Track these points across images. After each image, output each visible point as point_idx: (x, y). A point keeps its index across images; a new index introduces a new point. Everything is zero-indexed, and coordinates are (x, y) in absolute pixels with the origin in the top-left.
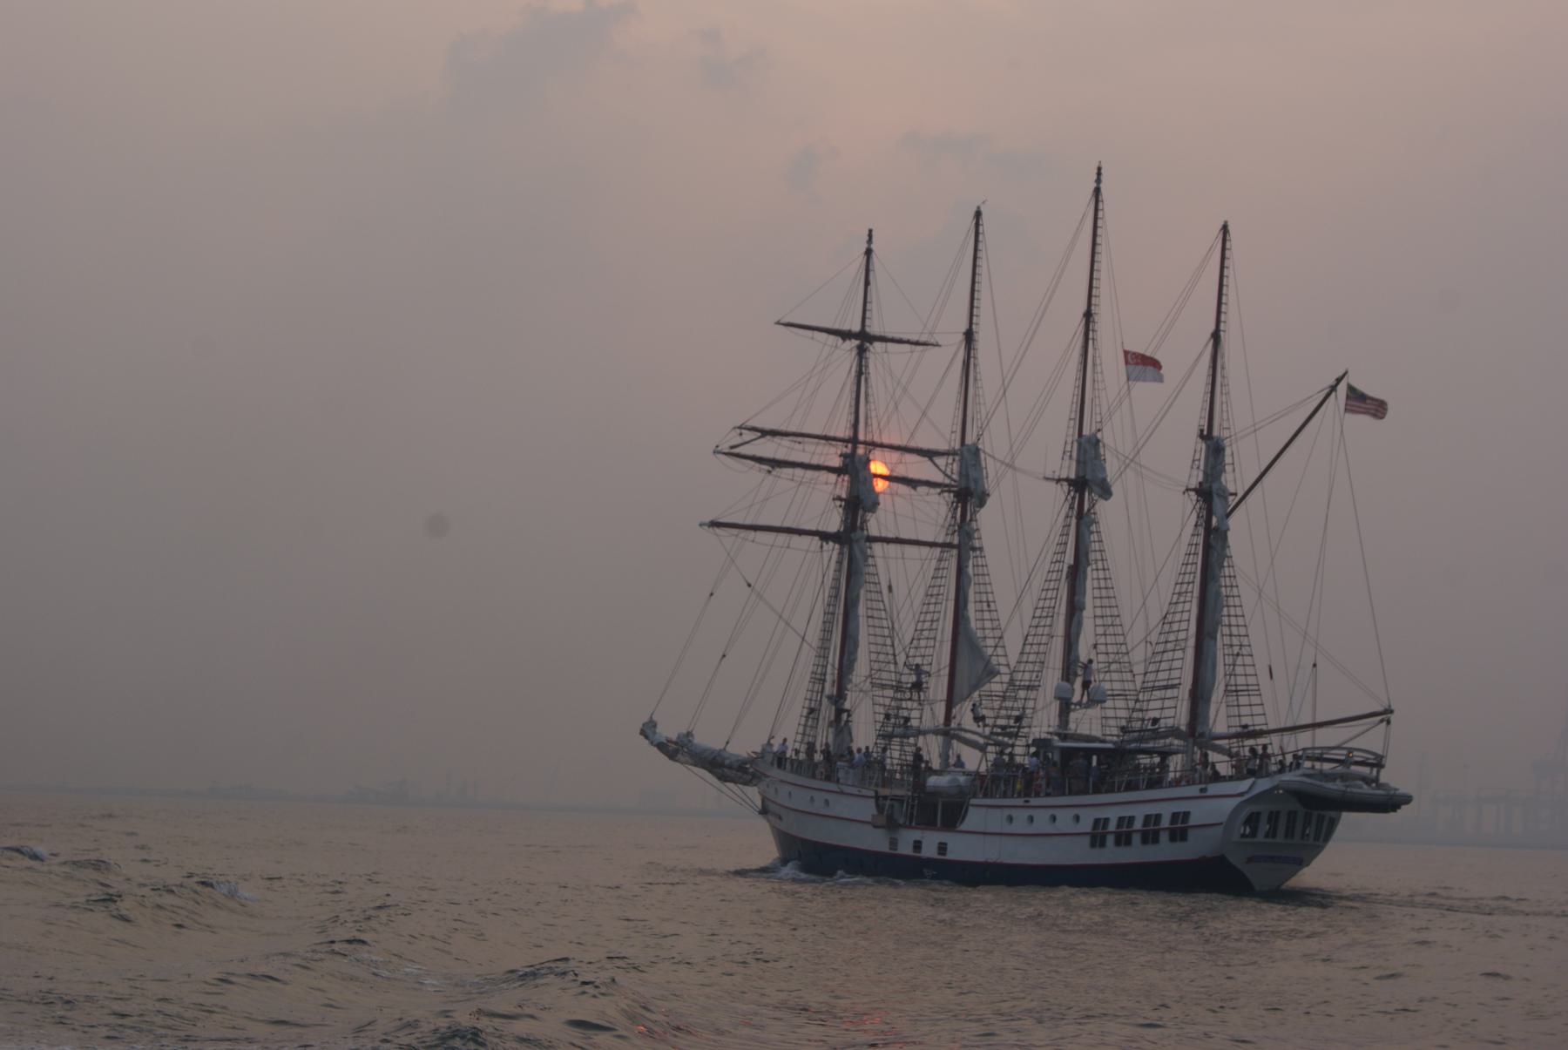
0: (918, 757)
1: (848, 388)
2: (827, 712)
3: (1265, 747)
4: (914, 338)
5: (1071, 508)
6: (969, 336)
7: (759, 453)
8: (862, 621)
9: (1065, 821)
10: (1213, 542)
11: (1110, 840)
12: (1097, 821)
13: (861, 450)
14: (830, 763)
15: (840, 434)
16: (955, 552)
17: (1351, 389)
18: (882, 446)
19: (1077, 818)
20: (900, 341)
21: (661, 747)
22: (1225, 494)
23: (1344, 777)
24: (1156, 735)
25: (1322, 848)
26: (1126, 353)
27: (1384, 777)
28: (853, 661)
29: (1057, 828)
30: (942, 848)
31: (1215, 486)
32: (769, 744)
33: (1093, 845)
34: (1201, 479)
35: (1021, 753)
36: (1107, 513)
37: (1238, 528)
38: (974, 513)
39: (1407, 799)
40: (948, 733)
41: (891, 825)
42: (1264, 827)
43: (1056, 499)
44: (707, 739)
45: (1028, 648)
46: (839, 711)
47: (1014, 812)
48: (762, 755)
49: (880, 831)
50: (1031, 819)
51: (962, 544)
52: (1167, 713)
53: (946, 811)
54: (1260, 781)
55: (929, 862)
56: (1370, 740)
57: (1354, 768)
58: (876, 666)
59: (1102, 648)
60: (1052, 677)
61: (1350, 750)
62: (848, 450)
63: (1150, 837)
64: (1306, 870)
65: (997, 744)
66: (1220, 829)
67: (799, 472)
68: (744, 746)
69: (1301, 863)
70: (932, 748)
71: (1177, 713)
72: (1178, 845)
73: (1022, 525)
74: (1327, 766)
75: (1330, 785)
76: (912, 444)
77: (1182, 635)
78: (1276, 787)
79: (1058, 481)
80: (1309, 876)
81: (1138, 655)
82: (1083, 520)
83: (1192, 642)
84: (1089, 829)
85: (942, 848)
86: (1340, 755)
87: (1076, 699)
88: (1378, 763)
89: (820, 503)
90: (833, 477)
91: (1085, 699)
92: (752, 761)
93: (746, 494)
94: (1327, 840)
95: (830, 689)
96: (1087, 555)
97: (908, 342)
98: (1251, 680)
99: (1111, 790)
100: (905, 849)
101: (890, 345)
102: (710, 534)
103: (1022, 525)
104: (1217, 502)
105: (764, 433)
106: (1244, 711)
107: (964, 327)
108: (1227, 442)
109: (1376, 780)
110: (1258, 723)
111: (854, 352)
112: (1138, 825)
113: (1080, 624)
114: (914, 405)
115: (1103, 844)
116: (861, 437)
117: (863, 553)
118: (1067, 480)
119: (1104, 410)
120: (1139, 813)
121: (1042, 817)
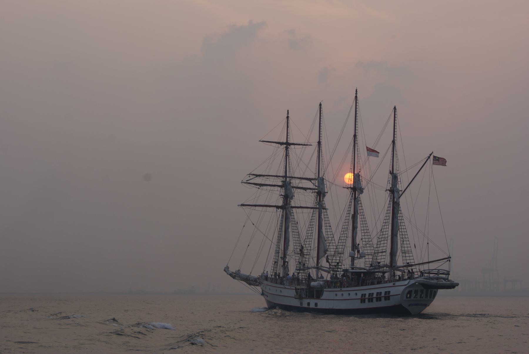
0: (309, 275)
1: (283, 160)
2: (281, 262)
3: (412, 270)
4: (303, 144)
5: (352, 196)
6: (319, 143)
7: (255, 182)
8: (291, 234)
9: (353, 295)
10: (395, 206)
11: (367, 300)
12: (362, 295)
13: (288, 179)
14: (279, 280)
15: (281, 175)
16: (318, 210)
17: (434, 157)
18: (295, 178)
19: (356, 294)
20: (299, 145)
21: (231, 275)
22: (398, 191)
23: (437, 279)
24: (380, 267)
25: (432, 301)
26: (367, 147)
27: (450, 278)
28: (288, 246)
29: (349, 298)
30: (316, 304)
31: (395, 189)
32: (264, 273)
33: (361, 302)
34: (391, 186)
35: (340, 275)
36: (364, 197)
37: (402, 201)
38: (359, 195)
39: (457, 285)
40: (318, 268)
41: (300, 298)
42: (413, 295)
43: (347, 194)
44: (245, 272)
45: (340, 241)
46: (284, 262)
47: (337, 293)
48: (261, 276)
49: (297, 300)
50: (342, 295)
51: (320, 207)
52: (382, 260)
53: (317, 293)
54: (411, 281)
55: (313, 309)
56: (445, 266)
57: (440, 275)
58: (295, 247)
59: (364, 240)
60: (348, 249)
61: (439, 270)
62: (284, 180)
63: (379, 299)
64: (428, 308)
65: (333, 271)
66: (399, 296)
67: (269, 187)
68: (256, 274)
69: (426, 305)
70: (313, 273)
71: (385, 259)
72: (387, 301)
73: (337, 203)
74: (431, 275)
75: (432, 281)
76: (304, 177)
77: (386, 236)
78: (416, 283)
79: (348, 188)
80: (428, 310)
81: (375, 241)
82: (356, 200)
83: (390, 238)
84: (360, 297)
85: (316, 304)
86: (436, 271)
87: (356, 256)
88: (448, 274)
89: (275, 197)
90: (279, 188)
91: (359, 256)
92: (258, 278)
93: (252, 194)
94: (434, 298)
95: (281, 255)
96: (357, 211)
97: (302, 145)
98: (409, 249)
99: (366, 285)
100: (305, 305)
101: (296, 146)
102: (241, 208)
103: (337, 203)
104: (396, 194)
105: (257, 176)
106: (408, 258)
107: (317, 140)
108: (398, 175)
109: (448, 279)
110: (412, 262)
111: (285, 149)
112: (375, 296)
113: (356, 233)
114: (303, 164)
115: (372, 301)
116: (288, 175)
117: (290, 212)
118: (350, 188)
119: (361, 164)
120: (375, 292)
121: (346, 294)
